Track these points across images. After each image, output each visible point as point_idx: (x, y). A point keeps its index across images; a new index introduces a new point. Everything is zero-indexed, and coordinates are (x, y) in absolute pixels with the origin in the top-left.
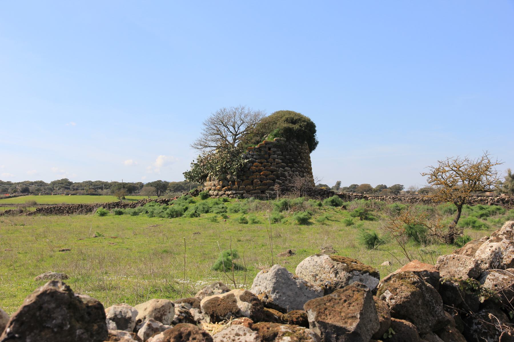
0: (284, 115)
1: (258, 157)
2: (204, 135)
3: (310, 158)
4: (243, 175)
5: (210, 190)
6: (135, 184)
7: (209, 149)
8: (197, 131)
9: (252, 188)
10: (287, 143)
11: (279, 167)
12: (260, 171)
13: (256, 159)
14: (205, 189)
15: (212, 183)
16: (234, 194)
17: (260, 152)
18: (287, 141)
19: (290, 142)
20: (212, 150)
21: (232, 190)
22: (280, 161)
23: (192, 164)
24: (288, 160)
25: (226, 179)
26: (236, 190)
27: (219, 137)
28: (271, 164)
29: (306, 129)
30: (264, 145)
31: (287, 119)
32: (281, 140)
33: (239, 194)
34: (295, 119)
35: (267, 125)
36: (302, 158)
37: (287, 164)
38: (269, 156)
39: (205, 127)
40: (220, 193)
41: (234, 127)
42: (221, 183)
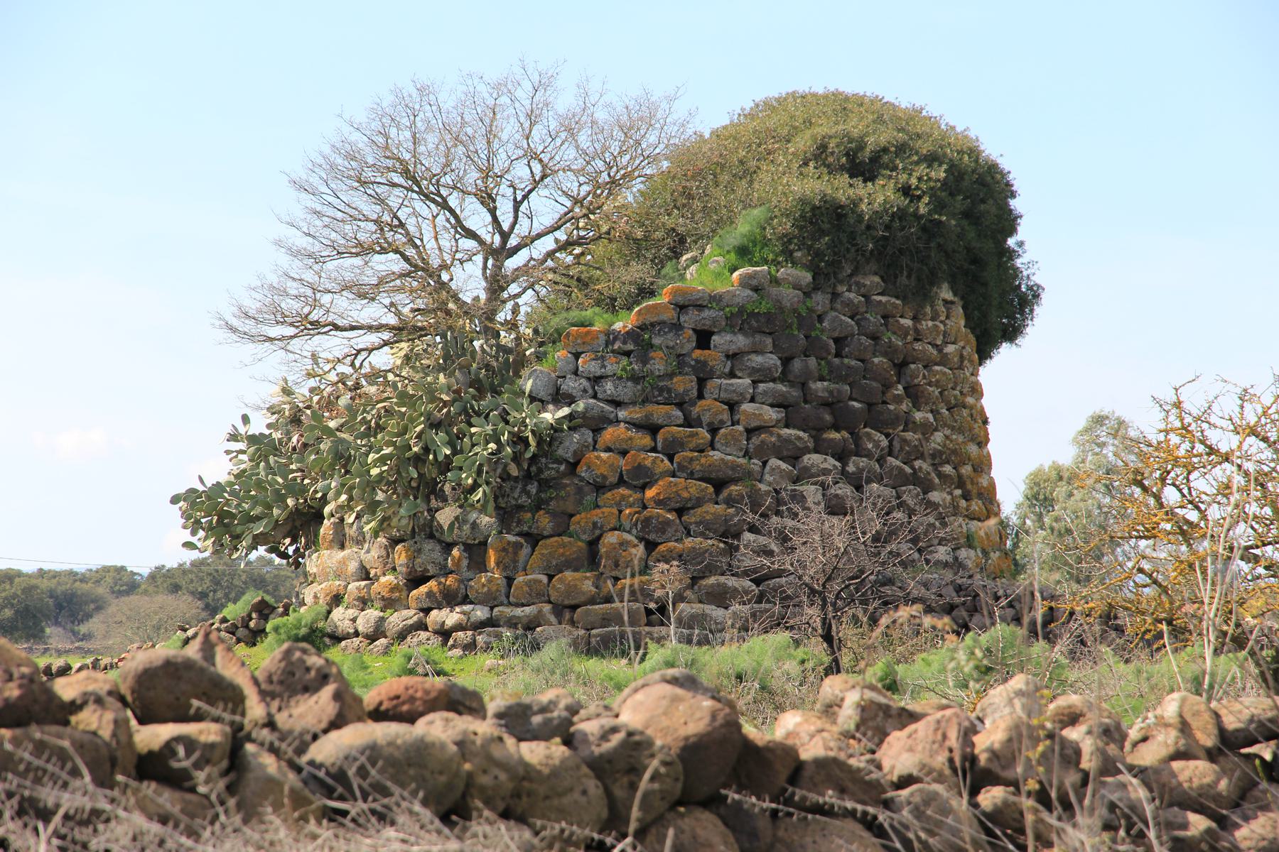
0: (809, 123)
1: (627, 391)
2: (296, 253)
3: (977, 391)
4: (538, 506)
5: (337, 599)
6: (83, 579)
7: (332, 345)
8: (257, 230)
9: (588, 587)
10: (820, 300)
11: (763, 453)
12: (641, 479)
13: (617, 404)
14: (308, 594)
15: (350, 558)
16: (479, 626)
17: (645, 360)
18: (816, 287)
19: (835, 296)
20: (363, 346)
21: (466, 600)
22: (772, 414)
23: (234, 437)
24: (826, 404)
25: (430, 531)
26: (490, 600)
27: (390, 263)
28: (714, 431)
29: (939, 206)
30: (670, 315)
31: (823, 147)
32: (775, 281)
33: (512, 623)
34: (866, 145)
35: (704, 179)
36: (914, 394)
37: (816, 430)
38: (701, 383)
39: (297, 206)
40: (397, 620)
41: (488, 200)
42: (400, 556)
